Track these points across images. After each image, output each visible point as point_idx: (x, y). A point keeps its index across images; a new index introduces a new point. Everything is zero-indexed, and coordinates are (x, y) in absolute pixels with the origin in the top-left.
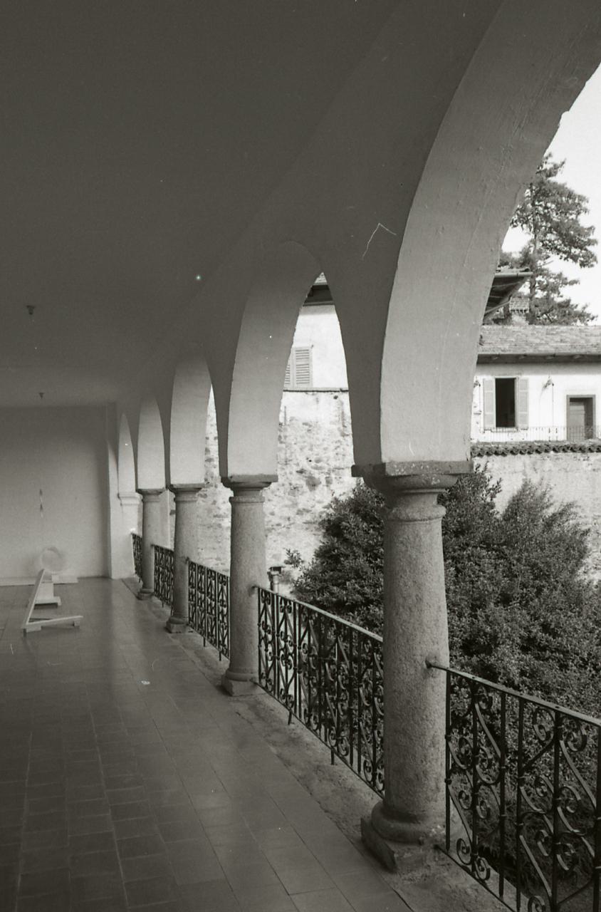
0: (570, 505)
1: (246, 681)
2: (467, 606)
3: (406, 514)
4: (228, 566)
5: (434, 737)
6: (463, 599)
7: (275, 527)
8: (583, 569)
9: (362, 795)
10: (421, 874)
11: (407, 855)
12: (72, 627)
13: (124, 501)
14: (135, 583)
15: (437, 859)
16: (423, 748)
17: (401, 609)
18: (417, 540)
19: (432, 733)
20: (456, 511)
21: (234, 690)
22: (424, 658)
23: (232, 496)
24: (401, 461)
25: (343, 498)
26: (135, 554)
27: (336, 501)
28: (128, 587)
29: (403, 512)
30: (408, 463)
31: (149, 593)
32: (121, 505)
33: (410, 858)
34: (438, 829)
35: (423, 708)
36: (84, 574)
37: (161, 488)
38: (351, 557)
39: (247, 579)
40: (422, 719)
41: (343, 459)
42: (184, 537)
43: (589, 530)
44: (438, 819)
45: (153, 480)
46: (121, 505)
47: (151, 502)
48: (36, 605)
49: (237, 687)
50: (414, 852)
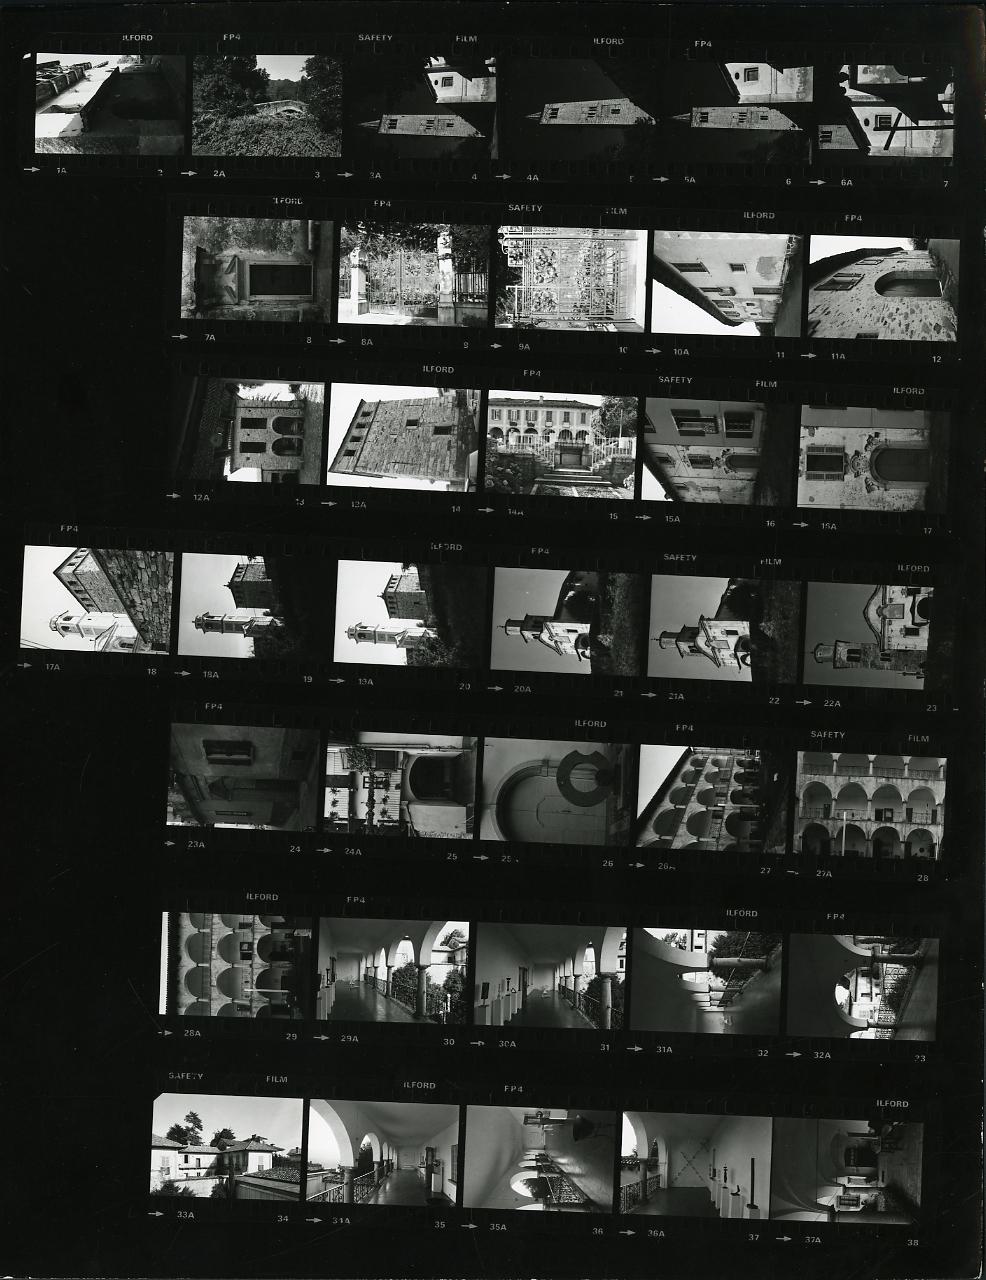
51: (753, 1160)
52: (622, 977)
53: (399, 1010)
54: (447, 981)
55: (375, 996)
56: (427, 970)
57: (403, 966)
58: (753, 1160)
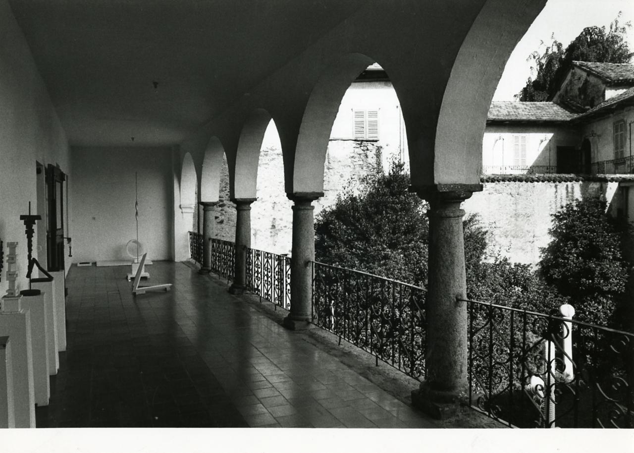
0: (474, 216)
1: (303, 321)
2: (413, 279)
3: (446, 214)
4: (289, 247)
5: (460, 341)
6: (410, 275)
7: (283, 228)
8: (484, 256)
9: (402, 381)
10: (454, 419)
11: (447, 409)
12: (164, 291)
13: (184, 210)
14: (192, 264)
15: (462, 411)
16: (454, 347)
17: (442, 268)
18: (452, 228)
19: (459, 338)
20: (404, 218)
21: (296, 326)
22: (455, 296)
23: (294, 205)
24: (446, 183)
25: (328, 210)
26: (191, 245)
27: (325, 211)
28: (189, 267)
29: (443, 213)
30: (449, 185)
31: (208, 270)
32: (182, 212)
33: (448, 410)
34: (463, 394)
35: (454, 324)
36: (155, 259)
37: (216, 201)
38: (336, 248)
39: (304, 257)
40: (454, 331)
41: (328, 184)
42: (243, 233)
43: (487, 231)
44: (462, 388)
45: (211, 194)
46: (182, 212)
47: (209, 210)
48: (141, 277)
49: (297, 325)
50: (450, 407)
51: (30, 202)
52: (290, 256)
53: (349, 377)
54: (553, 250)
55: (241, 324)
56: (468, 206)
57: (359, 191)
58: (30, 202)
